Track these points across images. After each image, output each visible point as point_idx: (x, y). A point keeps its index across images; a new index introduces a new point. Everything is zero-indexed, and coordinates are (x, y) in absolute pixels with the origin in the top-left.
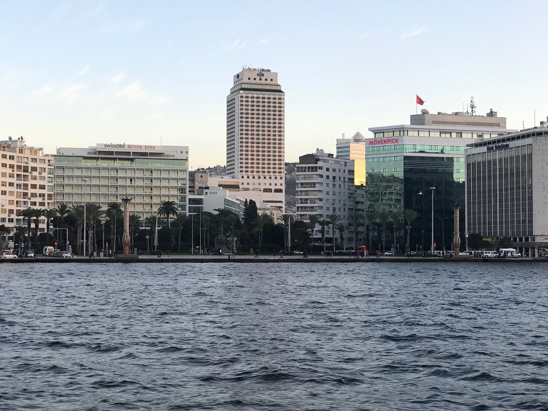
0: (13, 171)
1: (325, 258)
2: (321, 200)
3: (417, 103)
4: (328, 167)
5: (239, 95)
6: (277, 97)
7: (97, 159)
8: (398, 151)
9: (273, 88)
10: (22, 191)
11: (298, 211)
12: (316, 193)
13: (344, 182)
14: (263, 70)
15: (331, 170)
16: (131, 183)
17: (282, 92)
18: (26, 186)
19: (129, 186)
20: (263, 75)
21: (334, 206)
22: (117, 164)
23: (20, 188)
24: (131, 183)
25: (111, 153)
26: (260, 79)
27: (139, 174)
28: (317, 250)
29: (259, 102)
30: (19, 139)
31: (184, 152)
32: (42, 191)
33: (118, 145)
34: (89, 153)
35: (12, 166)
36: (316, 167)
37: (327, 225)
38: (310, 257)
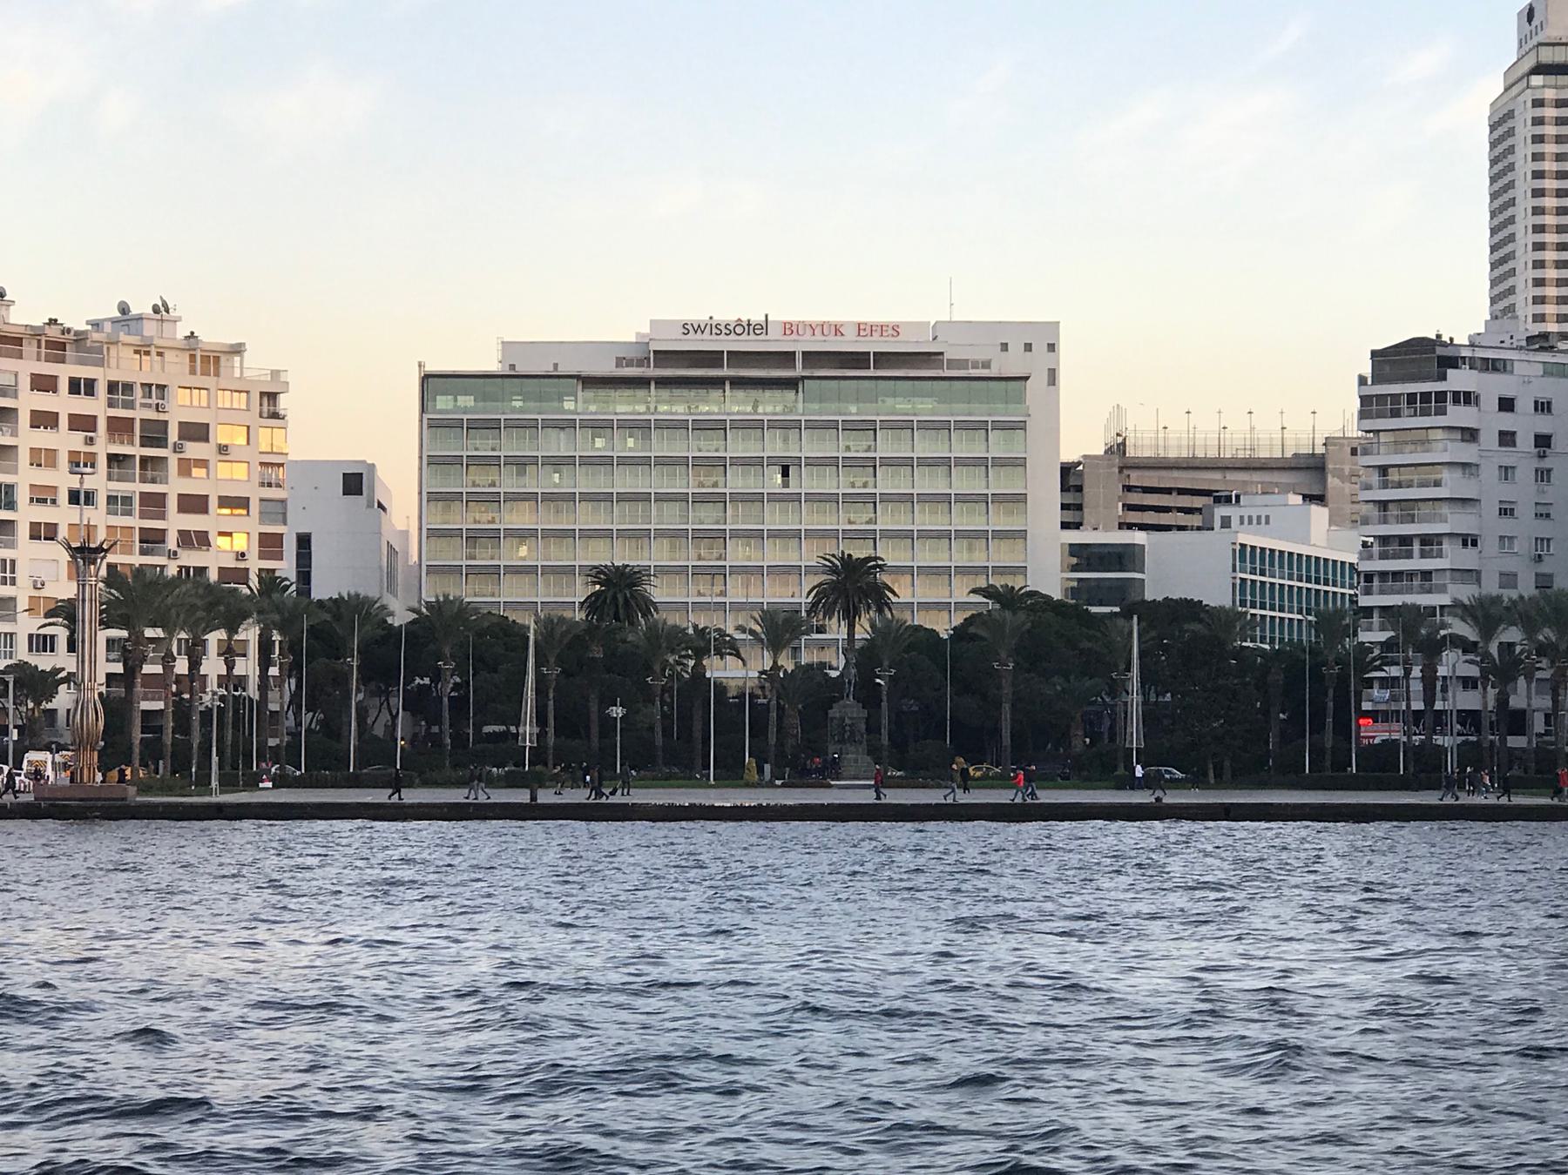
1: (1492, 800)
2: (1469, 541)
4: (1509, 394)
5: (1529, 96)
7: (642, 382)
10: (135, 522)
11: (1368, 592)
12: (1445, 509)
15: (1525, 405)
16: (786, 485)
18: (154, 504)
19: (774, 498)
21: (1544, 568)
22: (736, 405)
23: (129, 513)
24: (786, 485)
27: (810, 446)
30: (156, 310)
31: (1040, 348)
33: (739, 323)
34: (620, 362)
35: (83, 423)
36: (1441, 396)
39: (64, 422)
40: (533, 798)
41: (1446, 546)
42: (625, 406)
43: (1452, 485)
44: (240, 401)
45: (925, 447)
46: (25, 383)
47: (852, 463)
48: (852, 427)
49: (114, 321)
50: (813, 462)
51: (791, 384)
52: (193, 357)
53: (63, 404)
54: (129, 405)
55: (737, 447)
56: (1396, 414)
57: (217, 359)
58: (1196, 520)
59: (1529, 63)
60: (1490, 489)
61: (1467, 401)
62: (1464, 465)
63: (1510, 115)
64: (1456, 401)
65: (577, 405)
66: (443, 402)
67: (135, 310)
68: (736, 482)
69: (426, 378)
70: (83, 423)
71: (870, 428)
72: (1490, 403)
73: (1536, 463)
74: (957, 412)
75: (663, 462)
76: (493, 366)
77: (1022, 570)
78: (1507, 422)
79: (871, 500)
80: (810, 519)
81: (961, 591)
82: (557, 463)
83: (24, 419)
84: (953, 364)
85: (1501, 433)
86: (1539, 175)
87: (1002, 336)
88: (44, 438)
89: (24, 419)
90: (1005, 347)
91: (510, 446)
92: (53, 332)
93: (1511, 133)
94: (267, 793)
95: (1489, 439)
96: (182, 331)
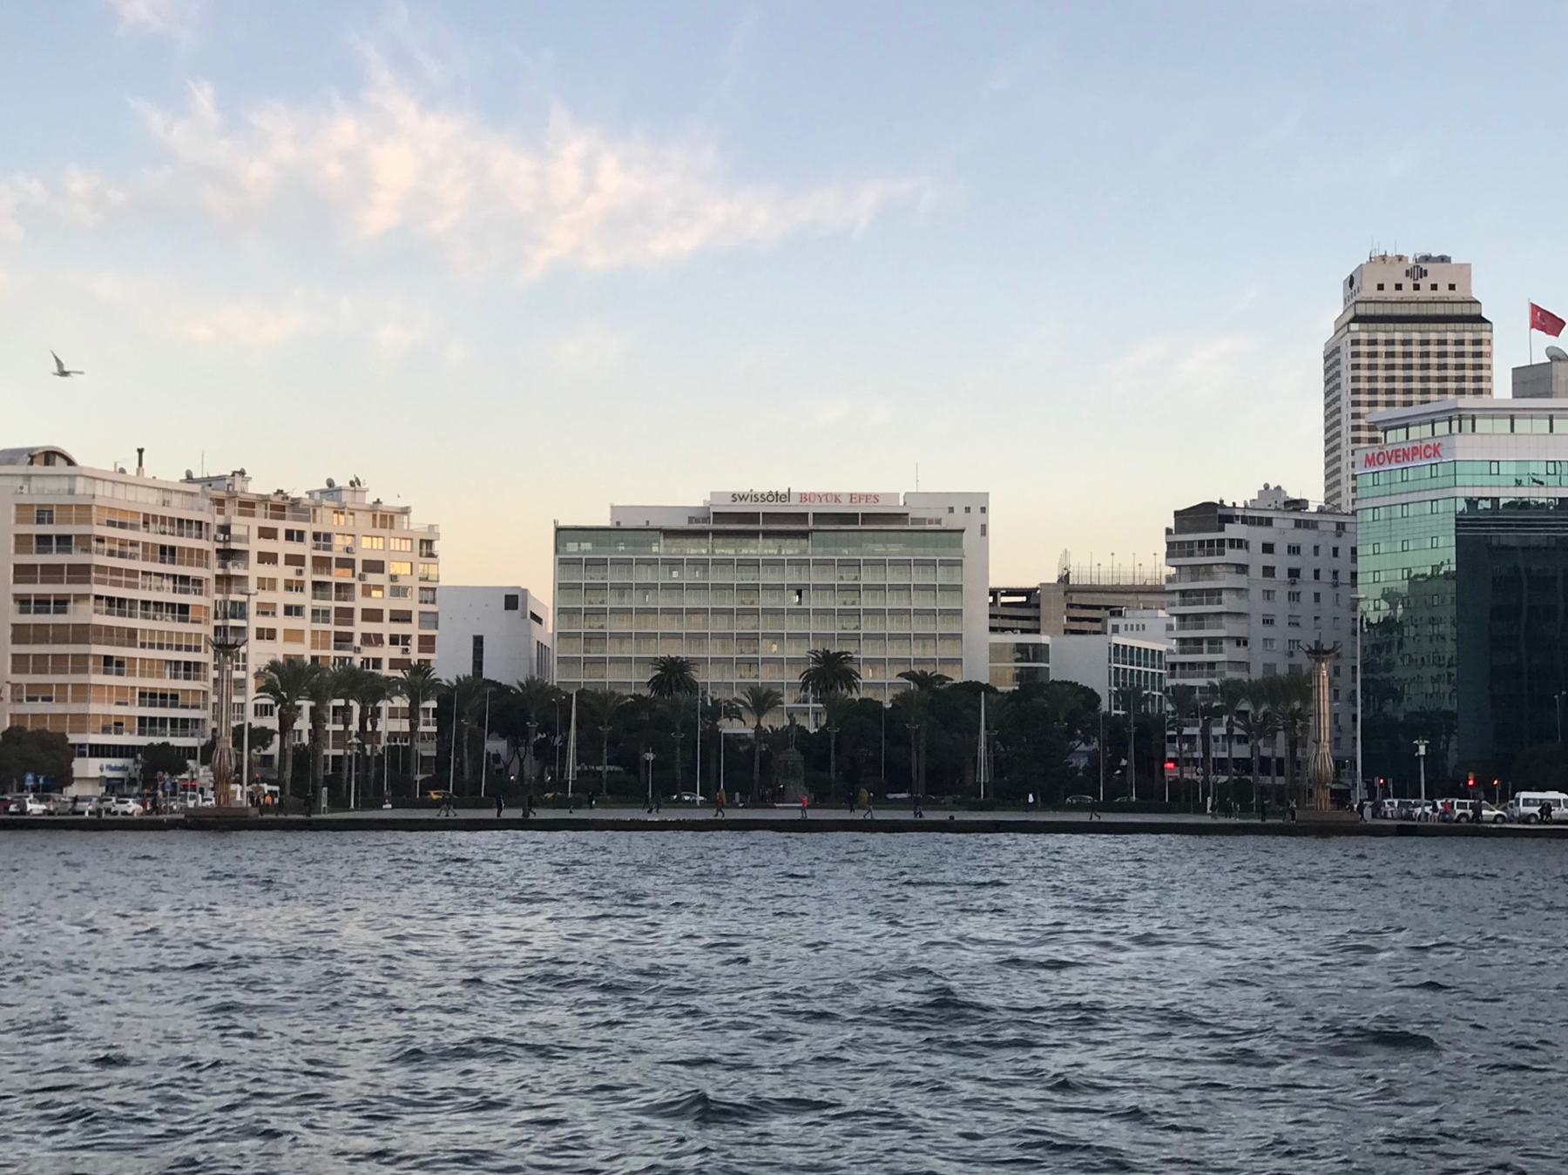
0: (300, 573)
2: (1241, 642)
3: (1534, 325)
4: (1270, 541)
5: (1349, 338)
6: (1468, 336)
8: (1440, 482)
9: (1458, 310)
10: (332, 628)
11: (1172, 676)
13: (1336, 585)
14: (1427, 259)
15: (1281, 548)
17: (1486, 321)
18: (345, 615)
19: (792, 612)
20: (1424, 273)
25: (752, 517)
26: (1417, 287)
27: (814, 577)
28: (1185, 797)
29: (1409, 355)
30: (352, 484)
31: (976, 510)
32: (400, 629)
33: (770, 494)
34: (691, 520)
35: (293, 560)
36: (1221, 542)
37: (317, 695)
38: (930, 816)
39: (281, 559)
40: (525, 814)
41: (1225, 644)
42: (694, 549)
43: (1229, 603)
44: (406, 545)
45: (893, 577)
46: (254, 532)
47: (844, 589)
48: (844, 564)
49: (322, 492)
50: (816, 587)
51: (804, 535)
52: (374, 516)
53: (281, 547)
54: (328, 548)
55: (768, 577)
56: (1191, 554)
57: (392, 518)
58: (1097, 626)
59: (1350, 315)
60: (1257, 606)
61: (1240, 546)
62: (1238, 590)
63: (1337, 350)
64: (1232, 546)
65: (659, 549)
66: (572, 547)
67: (338, 484)
68: (765, 601)
69: (559, 530)
70: (293, 560)
71: (856, 564)
72: (1256, 547)
73: (1289, 588)
74: (919, 554)
75: (716, 587)
76: (607, 523)
77: (959, 661)
78: (1268, 560)
79: (856, 613)
80: (814, 627)
81: (891, 676)
82: (645, 588)
83: (253, 557)
84: (915, 521)
85: (1265, 568)
86: (1356, 391)
87: (950, 503)
88: (267, 571)
89: (253, 557)
90: (951, 510)
91: (613, 577)
92: (278, 500)
93: (1338, 362)
94: (388, 811)
95: (1256, 572)
96: (370, 499)
